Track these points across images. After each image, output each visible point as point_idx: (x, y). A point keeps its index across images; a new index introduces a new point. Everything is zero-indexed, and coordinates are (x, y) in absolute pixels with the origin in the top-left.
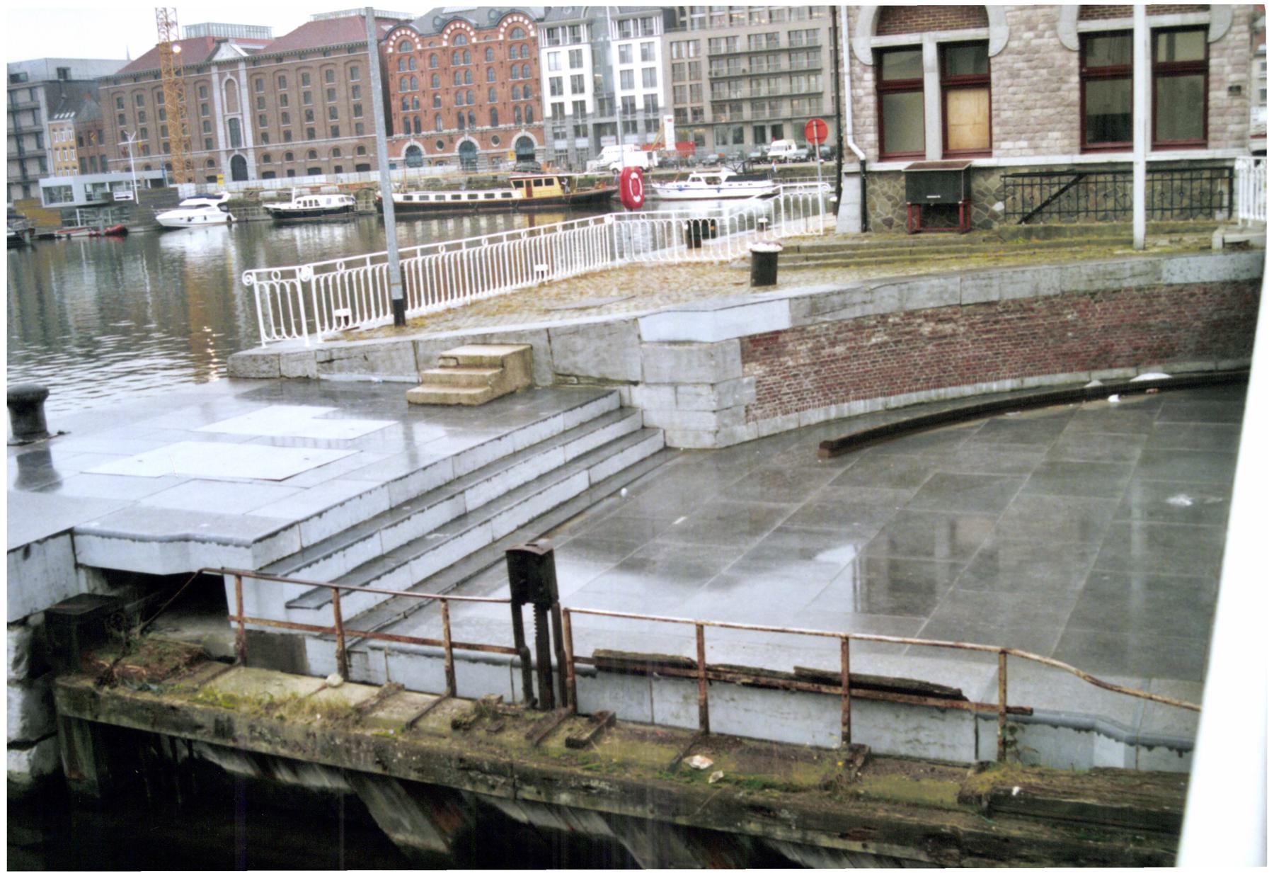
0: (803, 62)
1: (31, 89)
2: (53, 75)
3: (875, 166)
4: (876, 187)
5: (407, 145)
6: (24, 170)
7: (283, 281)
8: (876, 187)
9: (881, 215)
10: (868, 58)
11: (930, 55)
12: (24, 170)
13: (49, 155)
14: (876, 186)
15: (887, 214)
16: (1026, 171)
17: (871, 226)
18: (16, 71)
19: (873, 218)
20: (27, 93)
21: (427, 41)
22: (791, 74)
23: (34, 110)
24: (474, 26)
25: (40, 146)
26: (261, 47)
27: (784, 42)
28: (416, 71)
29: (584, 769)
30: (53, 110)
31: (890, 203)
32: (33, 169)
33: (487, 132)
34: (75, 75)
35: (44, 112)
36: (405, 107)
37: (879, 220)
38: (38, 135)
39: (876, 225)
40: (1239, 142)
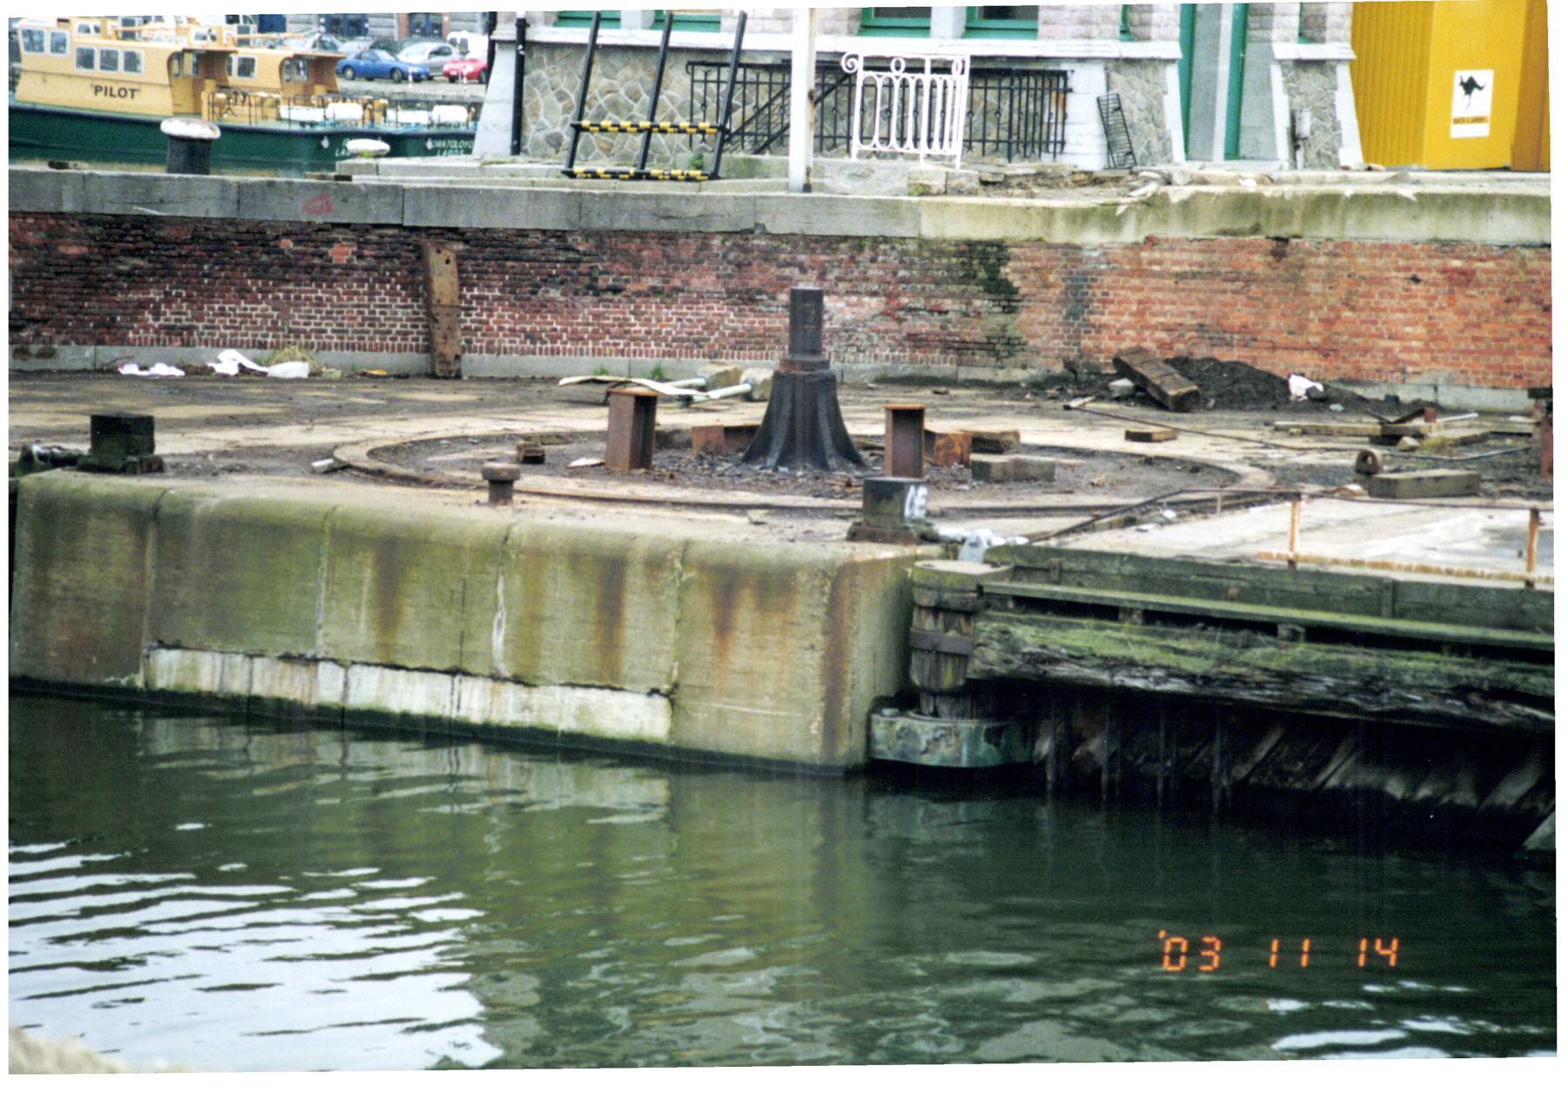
4: (544, 74)
7: (908, 76)
8: (544, 74)
9: (544, 127)
14: (541, 73)
15: (555, 125)
16: (768, 60)
17: (527, 146)
19: (531, 133)
29: (804, 1026)
31: (560, 106)
37: (541, 136)
39: (536, 145)
40: (1083, 29)
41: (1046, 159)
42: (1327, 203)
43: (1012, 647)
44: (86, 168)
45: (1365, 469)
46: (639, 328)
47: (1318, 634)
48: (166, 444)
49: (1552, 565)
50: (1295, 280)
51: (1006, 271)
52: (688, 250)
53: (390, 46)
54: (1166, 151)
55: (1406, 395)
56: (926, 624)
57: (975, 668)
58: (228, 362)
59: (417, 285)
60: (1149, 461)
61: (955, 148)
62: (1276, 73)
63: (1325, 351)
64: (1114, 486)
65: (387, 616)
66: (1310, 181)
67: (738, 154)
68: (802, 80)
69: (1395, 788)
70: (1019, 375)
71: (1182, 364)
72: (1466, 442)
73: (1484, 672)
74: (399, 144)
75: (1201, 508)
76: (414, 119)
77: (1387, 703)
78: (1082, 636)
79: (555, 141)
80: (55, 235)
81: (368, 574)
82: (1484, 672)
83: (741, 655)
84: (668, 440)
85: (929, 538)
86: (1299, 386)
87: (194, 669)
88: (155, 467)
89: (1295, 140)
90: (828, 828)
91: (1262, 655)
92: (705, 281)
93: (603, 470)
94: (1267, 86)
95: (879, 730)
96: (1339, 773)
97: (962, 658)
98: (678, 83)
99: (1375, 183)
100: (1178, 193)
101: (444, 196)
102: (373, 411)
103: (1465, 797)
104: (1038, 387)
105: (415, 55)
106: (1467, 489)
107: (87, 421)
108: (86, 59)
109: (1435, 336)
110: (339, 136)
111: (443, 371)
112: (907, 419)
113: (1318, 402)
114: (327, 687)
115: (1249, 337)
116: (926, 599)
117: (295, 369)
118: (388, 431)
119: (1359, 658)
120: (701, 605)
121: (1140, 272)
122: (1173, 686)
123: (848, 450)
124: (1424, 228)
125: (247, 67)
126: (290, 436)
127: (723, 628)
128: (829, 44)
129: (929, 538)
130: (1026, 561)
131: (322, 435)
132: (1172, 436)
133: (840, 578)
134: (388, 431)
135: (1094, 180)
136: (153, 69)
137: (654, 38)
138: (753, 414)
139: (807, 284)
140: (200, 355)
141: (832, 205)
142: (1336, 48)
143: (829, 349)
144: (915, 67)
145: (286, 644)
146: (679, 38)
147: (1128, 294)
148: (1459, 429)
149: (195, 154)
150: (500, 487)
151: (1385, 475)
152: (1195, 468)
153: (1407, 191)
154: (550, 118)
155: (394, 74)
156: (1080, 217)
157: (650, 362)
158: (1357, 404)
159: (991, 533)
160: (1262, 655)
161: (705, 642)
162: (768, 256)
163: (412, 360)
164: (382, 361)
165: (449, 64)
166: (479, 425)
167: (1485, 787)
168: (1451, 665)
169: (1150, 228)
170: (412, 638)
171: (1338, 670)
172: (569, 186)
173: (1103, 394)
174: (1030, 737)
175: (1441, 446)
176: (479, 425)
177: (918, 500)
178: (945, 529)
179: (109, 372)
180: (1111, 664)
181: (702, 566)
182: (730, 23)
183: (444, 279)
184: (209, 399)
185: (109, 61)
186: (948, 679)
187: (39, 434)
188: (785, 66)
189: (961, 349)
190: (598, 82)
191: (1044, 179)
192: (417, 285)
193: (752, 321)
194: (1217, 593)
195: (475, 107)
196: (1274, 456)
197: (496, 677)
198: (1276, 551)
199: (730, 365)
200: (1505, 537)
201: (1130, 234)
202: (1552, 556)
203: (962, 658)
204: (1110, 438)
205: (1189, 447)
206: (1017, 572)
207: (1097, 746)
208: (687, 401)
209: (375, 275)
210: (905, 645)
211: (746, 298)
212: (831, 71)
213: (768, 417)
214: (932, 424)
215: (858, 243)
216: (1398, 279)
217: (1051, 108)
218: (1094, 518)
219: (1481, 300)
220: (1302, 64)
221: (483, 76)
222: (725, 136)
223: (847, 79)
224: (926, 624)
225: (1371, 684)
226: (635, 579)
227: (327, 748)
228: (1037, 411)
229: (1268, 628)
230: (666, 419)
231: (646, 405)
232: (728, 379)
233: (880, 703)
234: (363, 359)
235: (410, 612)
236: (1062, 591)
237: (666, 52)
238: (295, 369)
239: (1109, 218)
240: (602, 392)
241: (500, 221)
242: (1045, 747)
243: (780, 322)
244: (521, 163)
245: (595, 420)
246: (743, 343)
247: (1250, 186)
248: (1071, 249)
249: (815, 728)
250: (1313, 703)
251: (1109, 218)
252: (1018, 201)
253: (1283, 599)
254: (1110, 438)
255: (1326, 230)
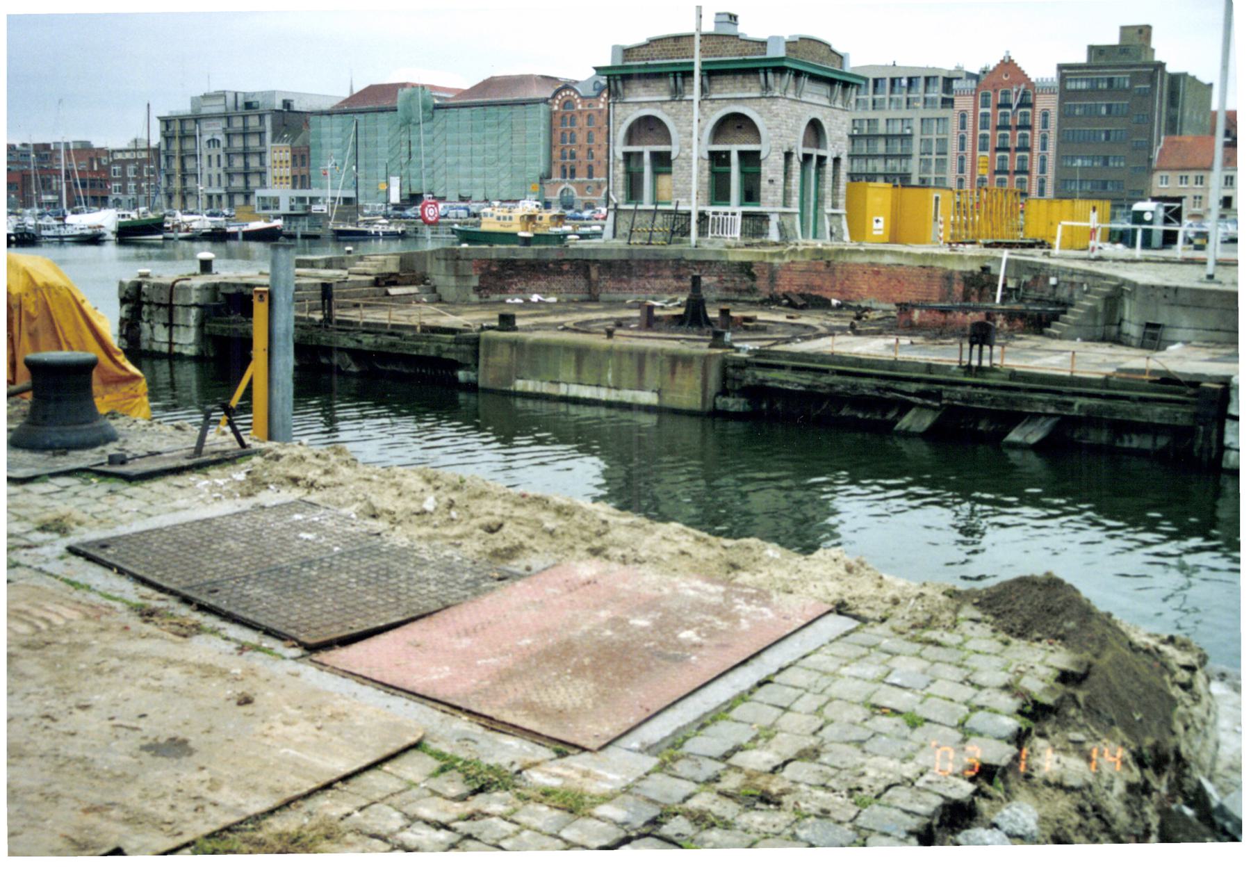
0: (898, 148)
1: (261, 117)
2: (278, 105)
3: (622, 207)
5: (563, 187)
6: (247, 182)
10: (620, 156)
11: (647, 157)
12: (247, 182)
13: (268, 170)
14: (621, 216)
18: (250, 100)
19: (619, 232)
20: (257, 118)
21: (587, 102)
22: (886, 157)
23: (261, 134)
24: (170, 190)
25: (262, 163)
26: (450, 96)
27: (882, 129)
28: (575, 128)
30: (277, 136)
32: (254, 181)
33: (583, 182)
34: (297, 106)
35: (268, 136)
36: (564, 157)
38: (261, 154)
41: (763, 239)
42: (840, 252)
43: (755, 377)
44: (498, 246)
45: (852, 327)
46: (648, 286)
47: (840, 373)
48: (519, 323)
49: (1237, 362)
50: (832, 272)
51: (753, 270)
52: (663, 264)
53: (580, 211)
54: (796, 237)
55: (863, 305)
56: (731, 371)
57: (745, 383)
58: (535, 298)
59: (587, 276)
60: (793, 325)
61: (737, 235)
62: (826, 218)
63: (841, 292)
64: (783, 332)
65: (579, 371)
66: (835, 245)
67: (677, 237)
68: (694, 218)
69: (860, 415)
70: (757, 299)
71: (802, 296)
72: (879, 319)
73: (883, 383)
74: (583, 236)
75: (807, 338)
76: (587, 230)
77: (858, 393)
78: (775, 374)
79: (625, 235)
80: (490, 265)
81: (573, 358)
82: (883, 383)
83: (678, 381)
84: (658, 319)
85: (732, 347)
86: (834, 302)
87: (526, 385)
88: (515, 329)
89: (832, 234)
90: (703, 430)
91: (825, 379)
92: (667, 273)
93: (639, 329)
94: (823, 221)
95: (718, 401)
96: (845, 412)
97: (740, 381)
98: (659, 219)
99: (853, 246)
100: (800, 248)
101: (595, 251)
102: (575, 312)
103: (878, 417)
104: (762, 302)
105: (587, 214)
106: (879, 333)
107: (497, 316)
108: (499, 218)
109: (870, 288)
110: (565, 235)
111: (594, 299)
112: (724, 312)
113: (839, 307)
114: (563, 390)
115: (820, 288)
116: (731, 364)
117: (553, 299)
118: (579, 317)
119: (851, 380)
120: (667, 365)
121: (790, 270)
122: (800, 388)
123: (709, 322)
124: (866, 259)
125: (541, 218)
126: (552, 319)
127: (673, 373)
128: (701, 208)
129: (732, 347)
130: (759, 353)
131: (561, 319)
132: (799, 317)
133: (706, 359)
134: (579, 317)
135: (776, 244)
136: (516, 220)
137: (653, 207)
138: (681, 311)
139: (696, 273)
140: (528, 296)
141: (704, 251)
142: (842, 211)
143: (703, 292)
144: (726, 214)
145: (551, 378)
146: (660, 207)
147: (787, 276)
148: (877, 315)
149: (527, 241)
150: (610, 334)
151: (858, 328)
152: (806, 327)
153: (862, 248)
154: (623, 228)
155: (581, 219)
156: (773, 255)
157: (650, 295)
158: (850, 308)
159: (749, 346)
160: (825, 379)
161: (668, 377)
162: (685, 266)
163: (586, 296)
164: (576, 297)
165: (596, 215)
166: (604, 315)
167: (884, 415)
168: (875, 381)
169: (793, 258)
170: (586, 375)
171: (845, 383)
172: (628, 247)
173: (780, 304)
174: (761, 403)
175: (873, 320)
176: (604, 315)
177: (728, 336)
178: (737, 345)
179: (503, 302)
180: (782, 382)
181: (667, 356)
182: (674, 203)
183: (594, 274)
184: (529, 308)
185: (505, 218)
186: (737, 387)
187: (485, 320)
188: (689, 214)
189: (740, 291)
190: (637, 219)
191: (764, 244)
192: (587, 276)
193: (681, 284)
194: (812, 361)
195: (603, 226)
196: (828, 323)
197: (609, 387)
198: (828, 350)
199: (674, 296)
200: (889, 347)
201: (787, 260)
202: (1237, 355)
203: (740, 381)
204: (781, 318)
205: (804, 320)
206: (756, 356)
207: (779, 405)
208: (662, 308)
209: (575, 273)
210: (724, 377)
211: (679, 278)
212: (703, 216)
213: (686, 312)
214: (733, 314)
215: (710, 262)
216: (860, 273)
217: (764, 225)
218: (778, 341)
219: (883, 279)
220: (833, 215)
221: (605, 218)
222: (673, 233)
223: (707, 217)
224: (731, 371)
225: (854, 387)
226: (648, 359)
227: (563, 408)
228: (762, 310)
229: (826, 371)
230: (657, 313)
231: (651, 308)
232: (674, 300)
233: (717, 394)
234: (571, 296)
235: (585, 369)
236: (769, 361)
237: (656, 212)
238: (553, 299)
239: (781, 255)
240: (639, 305)
241: (610, 257)
242: (764, 406)
243: (688, 284)
244: (615, 241)
245: (636, 313)
246: (680, 290)
247: (820, 246)
248: (771, 264)
249: (700, 400)
250: (838, 393)
251: (781, 255)
252: (756, 250)
253: (831, 363)
254: (781, 318)
255: (841, 259)
